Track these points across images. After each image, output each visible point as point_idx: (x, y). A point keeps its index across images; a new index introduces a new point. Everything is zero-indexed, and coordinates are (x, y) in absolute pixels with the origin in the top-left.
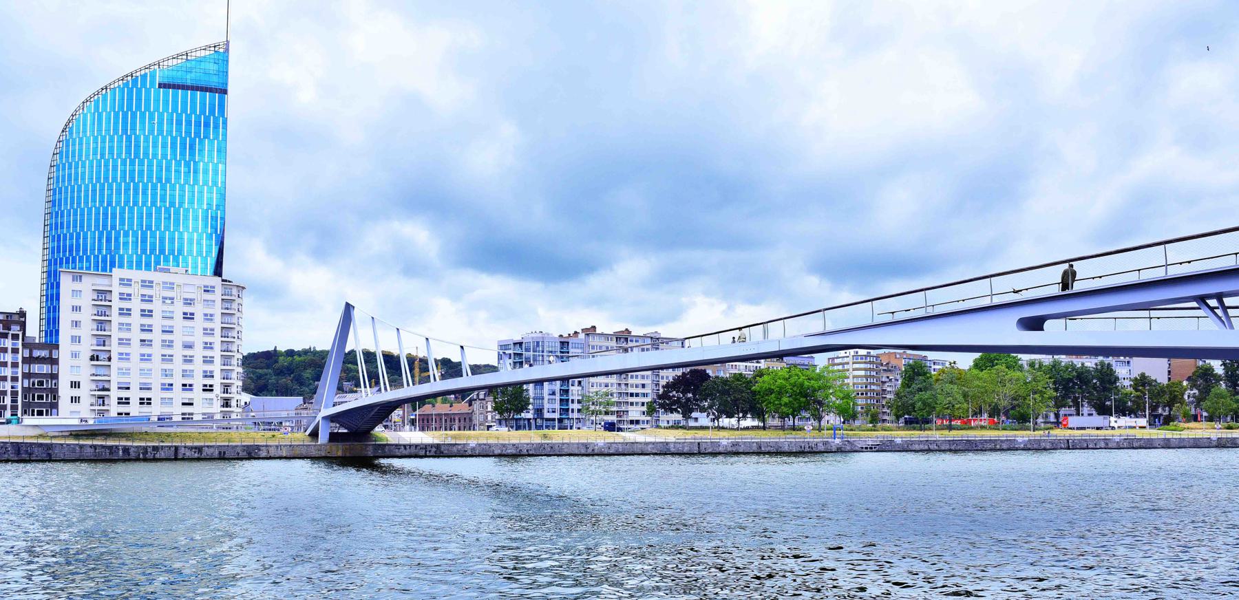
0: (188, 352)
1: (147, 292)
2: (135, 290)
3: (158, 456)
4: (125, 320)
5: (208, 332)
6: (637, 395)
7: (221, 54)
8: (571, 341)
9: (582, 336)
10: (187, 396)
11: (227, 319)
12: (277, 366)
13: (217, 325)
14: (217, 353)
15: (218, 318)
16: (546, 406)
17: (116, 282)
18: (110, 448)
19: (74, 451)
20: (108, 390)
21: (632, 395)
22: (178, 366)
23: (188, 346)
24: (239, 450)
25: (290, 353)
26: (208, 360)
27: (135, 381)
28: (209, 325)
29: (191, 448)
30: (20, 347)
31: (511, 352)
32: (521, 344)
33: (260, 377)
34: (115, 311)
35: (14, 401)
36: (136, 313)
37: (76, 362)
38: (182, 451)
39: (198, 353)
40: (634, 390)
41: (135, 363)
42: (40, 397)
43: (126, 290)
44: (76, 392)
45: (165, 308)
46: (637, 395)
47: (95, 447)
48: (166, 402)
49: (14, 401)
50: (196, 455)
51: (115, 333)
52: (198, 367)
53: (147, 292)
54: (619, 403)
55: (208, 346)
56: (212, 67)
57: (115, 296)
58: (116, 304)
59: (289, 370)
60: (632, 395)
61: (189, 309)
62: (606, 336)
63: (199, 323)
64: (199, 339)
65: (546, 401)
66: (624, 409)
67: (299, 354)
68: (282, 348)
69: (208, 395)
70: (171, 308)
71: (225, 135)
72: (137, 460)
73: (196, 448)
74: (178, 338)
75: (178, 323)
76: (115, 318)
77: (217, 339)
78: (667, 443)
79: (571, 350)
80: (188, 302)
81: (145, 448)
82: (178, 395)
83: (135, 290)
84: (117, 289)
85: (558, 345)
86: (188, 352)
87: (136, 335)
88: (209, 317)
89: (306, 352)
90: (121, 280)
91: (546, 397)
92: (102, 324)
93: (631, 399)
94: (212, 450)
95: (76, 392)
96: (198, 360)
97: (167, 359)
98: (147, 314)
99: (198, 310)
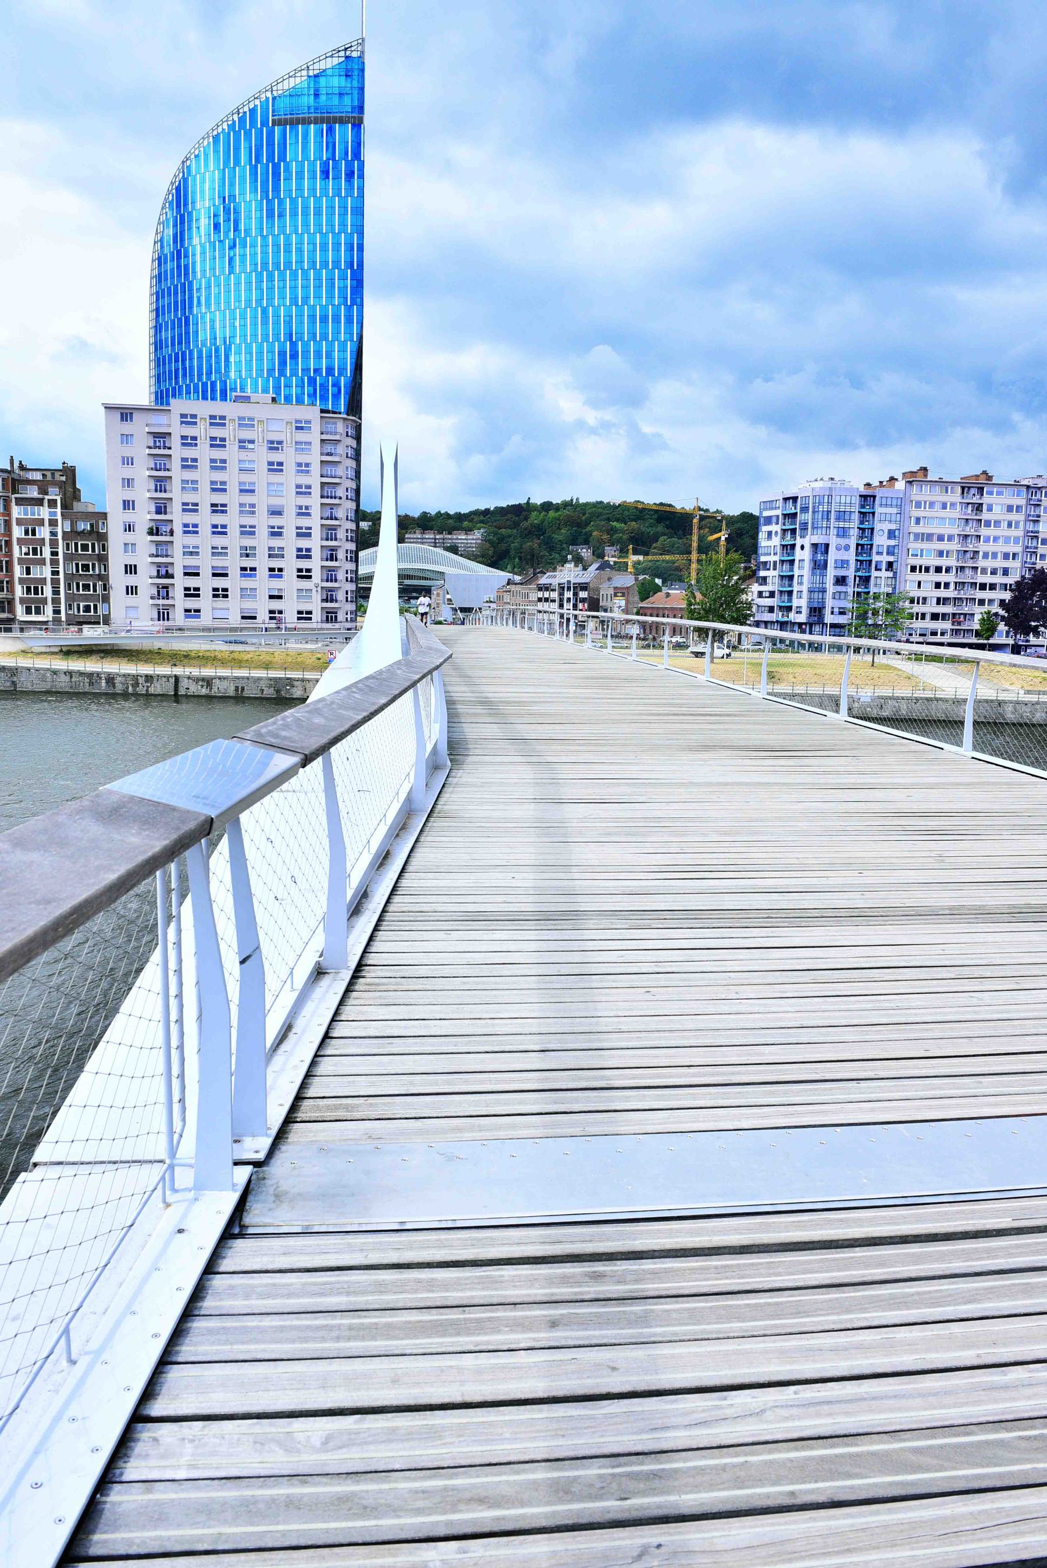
0: (276, 521)
1: (218, 432)
2: (202, 431)
3: (152, 690)
4: (189, 475)
5: (303, 491)
6: (993, 587)
7: (353, 68)
8: (879, 493)
9: (900, 485)
10: (276, 584)
11: (329, 470)
12: (525, 524)
13: (314, 480)
14: (315, 522)
15: (316, 469)
16: (829, 603)
17: (176, 420)
18: (90, 675)
19: (43, 679)
20: (172, 577)
21: (983, 587)
22: (262, 542)
23: (276, 512)
24: (263, 684)
25: (547, 506)
26: (304, 533)
27: (206, 563)
28: (304, 480)
29: (197, 680)
30: (59, 517)
31: (779, 512)
32: (795, 499)
33: (501, 540)
34: (176, 464)
35: (56, 592)
36: (204, 464)
37: (130, 537)
38: (184, 684)
39: (290, 522)
40: (988, 579)
41: (205, 540)
42: (86, 587)
43: (190, 431)
44: (131, 580)
45: (243, 455)
46: (993, 587)
47: (70, 673)
48: (247, 593)
49: (56, 592)
50: (204, 691)
51: (177, 495)
52: (290, 543)
53: (218, 432)
54: (957, 601)
55: (303, 512)
56: (337, 82)
57: (175, 441)
58: (177, 451)
59: (538, 531)
60: (983, 587)
61: (276, 457)
62: (943, 484)
63: (290, 477)
64: (290, 502)
65: (829, 595)
66: (966, 610)
67: (557, 507)
68: (538, 500)
69: (305, 584)
70: (251, 456)
71: (361, 189)
72: (125, 695)
73: (203, 680)
74: (262, 500)
75: (261, 478)
76: (177, 473)
77: (314, 501)
78: (1000, 703)
79: (879, 510)
80: (275, 446)
81: (135, 678)
82: (263, 583)
83: (202, 431)
84: (177, 430)
85: (856, 500)
86: (276, 521)
87: (205, 498)
88: (303, 468)
89: (566, 504)
90: (183, 416)
91: (831, 588)
92: (161, 483)
93: (980, 595)
94: (225, 684)
95: (131, 580)
96: (290, 532)
97: (248, 531)
98: (218, 465)
99: (288, 457)
